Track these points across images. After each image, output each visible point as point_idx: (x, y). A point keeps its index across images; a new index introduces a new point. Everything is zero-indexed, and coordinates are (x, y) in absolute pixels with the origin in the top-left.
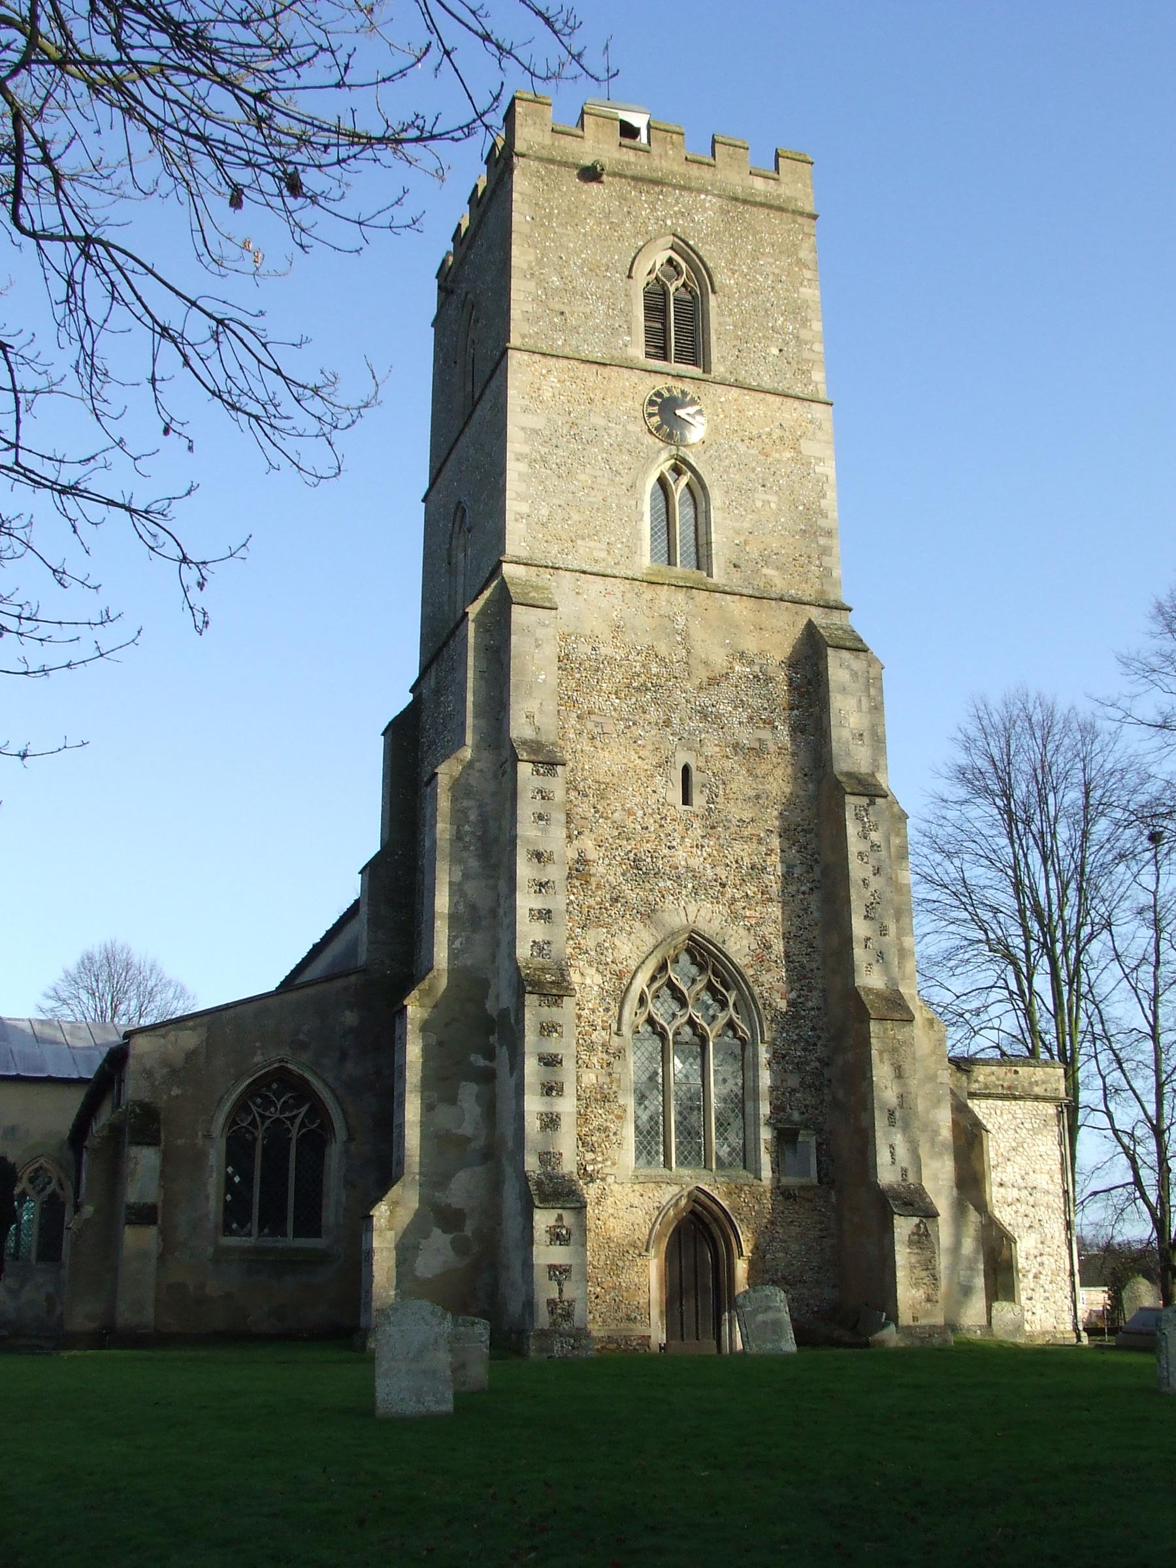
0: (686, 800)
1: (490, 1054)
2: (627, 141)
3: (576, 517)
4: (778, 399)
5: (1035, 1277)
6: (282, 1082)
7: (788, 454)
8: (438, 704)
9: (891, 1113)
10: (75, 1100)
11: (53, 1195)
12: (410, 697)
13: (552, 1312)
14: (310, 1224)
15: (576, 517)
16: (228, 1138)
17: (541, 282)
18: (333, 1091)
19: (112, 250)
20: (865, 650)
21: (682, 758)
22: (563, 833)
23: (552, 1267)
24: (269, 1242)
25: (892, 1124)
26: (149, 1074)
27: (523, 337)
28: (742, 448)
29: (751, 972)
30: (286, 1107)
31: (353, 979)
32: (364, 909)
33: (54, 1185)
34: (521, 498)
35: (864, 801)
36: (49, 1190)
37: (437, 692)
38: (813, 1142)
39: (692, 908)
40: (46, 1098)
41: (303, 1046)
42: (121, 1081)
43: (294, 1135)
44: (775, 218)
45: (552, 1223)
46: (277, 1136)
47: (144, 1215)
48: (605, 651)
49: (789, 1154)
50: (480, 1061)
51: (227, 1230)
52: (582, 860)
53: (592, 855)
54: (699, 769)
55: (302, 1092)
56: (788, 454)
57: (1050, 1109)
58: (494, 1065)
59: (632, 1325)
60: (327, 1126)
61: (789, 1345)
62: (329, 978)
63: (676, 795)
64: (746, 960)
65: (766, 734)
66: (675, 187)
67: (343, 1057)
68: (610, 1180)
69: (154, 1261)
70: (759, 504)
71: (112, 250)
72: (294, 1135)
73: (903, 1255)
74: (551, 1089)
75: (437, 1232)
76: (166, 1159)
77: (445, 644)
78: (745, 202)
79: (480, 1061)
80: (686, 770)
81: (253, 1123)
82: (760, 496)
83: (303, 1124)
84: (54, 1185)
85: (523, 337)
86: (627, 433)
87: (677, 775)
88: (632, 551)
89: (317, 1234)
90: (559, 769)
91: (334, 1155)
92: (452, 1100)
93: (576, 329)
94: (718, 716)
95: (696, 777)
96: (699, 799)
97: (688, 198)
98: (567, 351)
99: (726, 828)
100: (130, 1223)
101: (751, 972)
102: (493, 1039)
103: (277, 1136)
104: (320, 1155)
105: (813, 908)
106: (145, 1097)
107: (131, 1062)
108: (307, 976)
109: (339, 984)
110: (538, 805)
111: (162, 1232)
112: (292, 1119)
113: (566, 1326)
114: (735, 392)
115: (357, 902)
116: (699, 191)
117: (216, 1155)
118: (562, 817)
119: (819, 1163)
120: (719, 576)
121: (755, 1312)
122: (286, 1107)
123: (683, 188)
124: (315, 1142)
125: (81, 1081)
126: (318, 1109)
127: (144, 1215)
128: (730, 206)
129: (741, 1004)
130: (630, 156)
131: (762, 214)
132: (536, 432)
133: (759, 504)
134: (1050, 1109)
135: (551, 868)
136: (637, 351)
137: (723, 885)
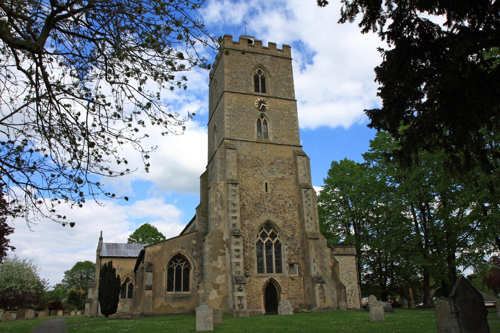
0: (266, 191)
1: (224, 249)
2: (249, 44)
3: (240, 128)
4: (285, 100)
5: (351, 295)
6: (179, 257)
7: (287, 112)
8: (212, 171)
9: (314, 260)
10: (134, 262)
11: (131, 283)
12: (206, 169)
13: (239, 307)
14: (186, 288)
15: (240, 128)
16: (168, 270)
17: (231, 76)
18: (191, 258)
19: (59, 105)
20: (306, 156)
21: (265, 182)
22: (239, 199)
23: (239, 297)
24: (178, 293)
25: (314, 262)
26: (150, 256)
27: (228, 88)
28: (277, 111)
29: (282, 229)
30: (180, 262)
31: (195, 233)
32: (197, 217)
33: (131, 281)
34: (228, 124)
35: (306, 190)
36: (130, 282)
37: (211, 168)
38: (297, 267)
39: (269, 215)
40: (128, 261)
41: (184, 248)
42: (144, 257)
43: (183, 268)
44: (283, 60)
45: (238, 287)
46: (179, 268)
47: (149, 288)
48: (248, 158)
49: (292, 270)
50: (222, 251)
51: (168, 290)
52: (244, 205)
53: (246, 204)
54: (269, 184)
55: (184, 259)
56: (287, 112)
57: (354, 257)
58: (225, 252)
59: (258, 309)
60: (190, 266)
61: (291, 313)
62: (189, 233)
63: (264, 190)
64: (281, 226)
65: (284, 175)
66: (260, 54)
67: (193, 251)
68: (252, 277)
69: (152, 298)
70: (281, 124)
71: (59, 105)
72: (183, 268)
73: (317, 293)
74: (238, 257)
75: (214, 290)
76: (154, 275)
77: (213, 157)
78: (276, 56)
79: (222, 251)
80: (266, 184)
81: (173, 266)
82: (281, 121)
83: (184, 266)
84: (131, 281)
85: (228, 88)
86: (251, 109)
87: (264, 185)
88: (253, 135)
89: (188, 291)
90: (238, 185)
91: (191, 272)
92: (216, 260)
93: (239, 86)
94: (273, 172)
95: (269, 186)
96: (269, 191)
97: (263, 56)
98: (237, 91)
99: (276, 197)
100: (146, 289)
101: (282, 229)
102: (225, 246)
103: (179, 268)
104: (188, 273)
105: (296, 214)
106: (149, 261)
107: (146, 253)
108: (186, 232)
109: (192, 234)
110: (233, 193)
111: (153, 291)
112: (182, 265)
113: (242, 310)
114: (274, 99)
115: (195, 215)
116: (266, 55)
117: (165, 274)
118: (239, 196)
119: (299, 271)
120: (271, 139)
121: (284, 306)
122: (180, 262)
123: (262, 54)
124: (187, 270)
125: (136, 257)
126: (187, 263)
127: (149, 288)
128: (272, 57)
129: (280, 236)
130: (250, 47)
131: (280, 59)
132: (231, 109)
133: (281, 124)
134: (354, 257)
135: (236, 207)
136: (253, 91)
137: (275, 210)
